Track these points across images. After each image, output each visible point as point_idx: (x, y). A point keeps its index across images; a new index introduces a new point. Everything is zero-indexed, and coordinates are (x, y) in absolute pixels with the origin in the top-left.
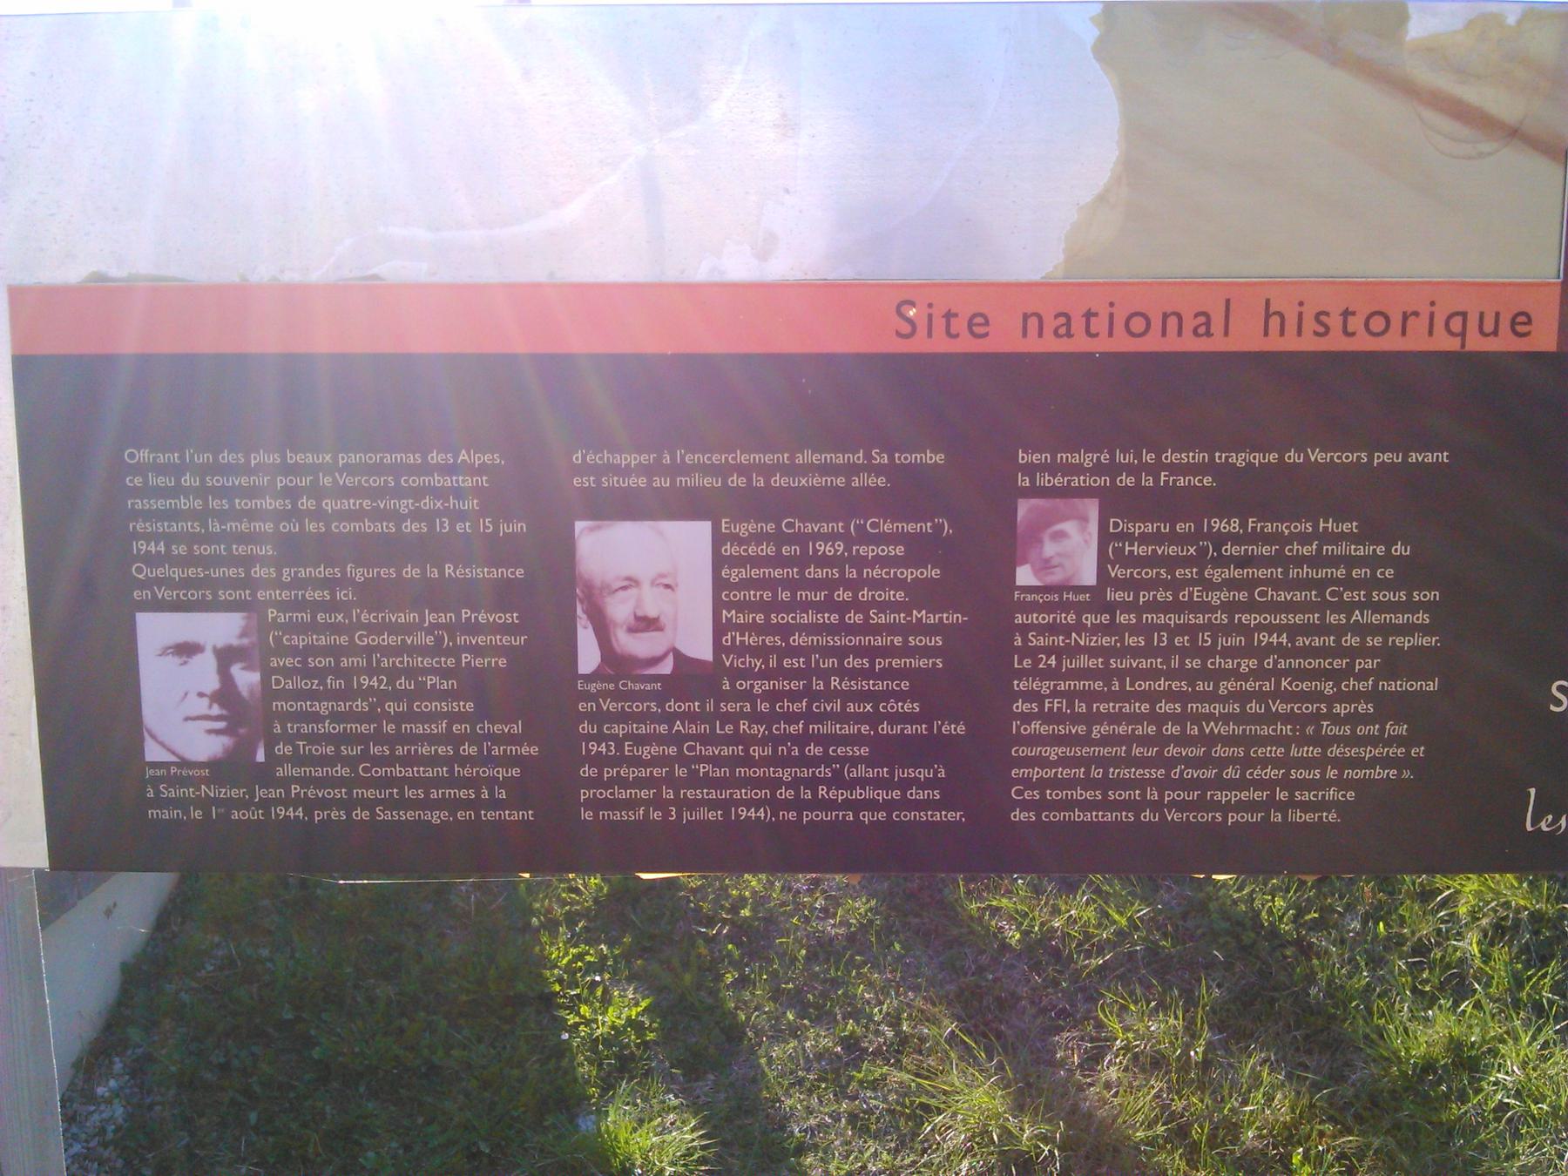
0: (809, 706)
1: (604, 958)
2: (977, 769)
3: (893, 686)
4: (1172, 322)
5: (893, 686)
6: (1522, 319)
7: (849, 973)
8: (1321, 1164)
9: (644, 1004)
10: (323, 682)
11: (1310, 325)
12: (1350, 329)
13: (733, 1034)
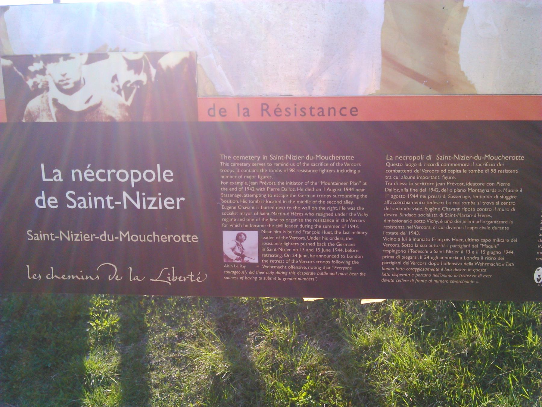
1: (111, 303)
2: (370, 245)
4: (332, 111)
6: (223, 110)
7: (188, 310)
8: (465, 380)
9: (117, 320)
10: (399, 214)
11: (299, 112)
12: (313, 114)
13: (144, 329)
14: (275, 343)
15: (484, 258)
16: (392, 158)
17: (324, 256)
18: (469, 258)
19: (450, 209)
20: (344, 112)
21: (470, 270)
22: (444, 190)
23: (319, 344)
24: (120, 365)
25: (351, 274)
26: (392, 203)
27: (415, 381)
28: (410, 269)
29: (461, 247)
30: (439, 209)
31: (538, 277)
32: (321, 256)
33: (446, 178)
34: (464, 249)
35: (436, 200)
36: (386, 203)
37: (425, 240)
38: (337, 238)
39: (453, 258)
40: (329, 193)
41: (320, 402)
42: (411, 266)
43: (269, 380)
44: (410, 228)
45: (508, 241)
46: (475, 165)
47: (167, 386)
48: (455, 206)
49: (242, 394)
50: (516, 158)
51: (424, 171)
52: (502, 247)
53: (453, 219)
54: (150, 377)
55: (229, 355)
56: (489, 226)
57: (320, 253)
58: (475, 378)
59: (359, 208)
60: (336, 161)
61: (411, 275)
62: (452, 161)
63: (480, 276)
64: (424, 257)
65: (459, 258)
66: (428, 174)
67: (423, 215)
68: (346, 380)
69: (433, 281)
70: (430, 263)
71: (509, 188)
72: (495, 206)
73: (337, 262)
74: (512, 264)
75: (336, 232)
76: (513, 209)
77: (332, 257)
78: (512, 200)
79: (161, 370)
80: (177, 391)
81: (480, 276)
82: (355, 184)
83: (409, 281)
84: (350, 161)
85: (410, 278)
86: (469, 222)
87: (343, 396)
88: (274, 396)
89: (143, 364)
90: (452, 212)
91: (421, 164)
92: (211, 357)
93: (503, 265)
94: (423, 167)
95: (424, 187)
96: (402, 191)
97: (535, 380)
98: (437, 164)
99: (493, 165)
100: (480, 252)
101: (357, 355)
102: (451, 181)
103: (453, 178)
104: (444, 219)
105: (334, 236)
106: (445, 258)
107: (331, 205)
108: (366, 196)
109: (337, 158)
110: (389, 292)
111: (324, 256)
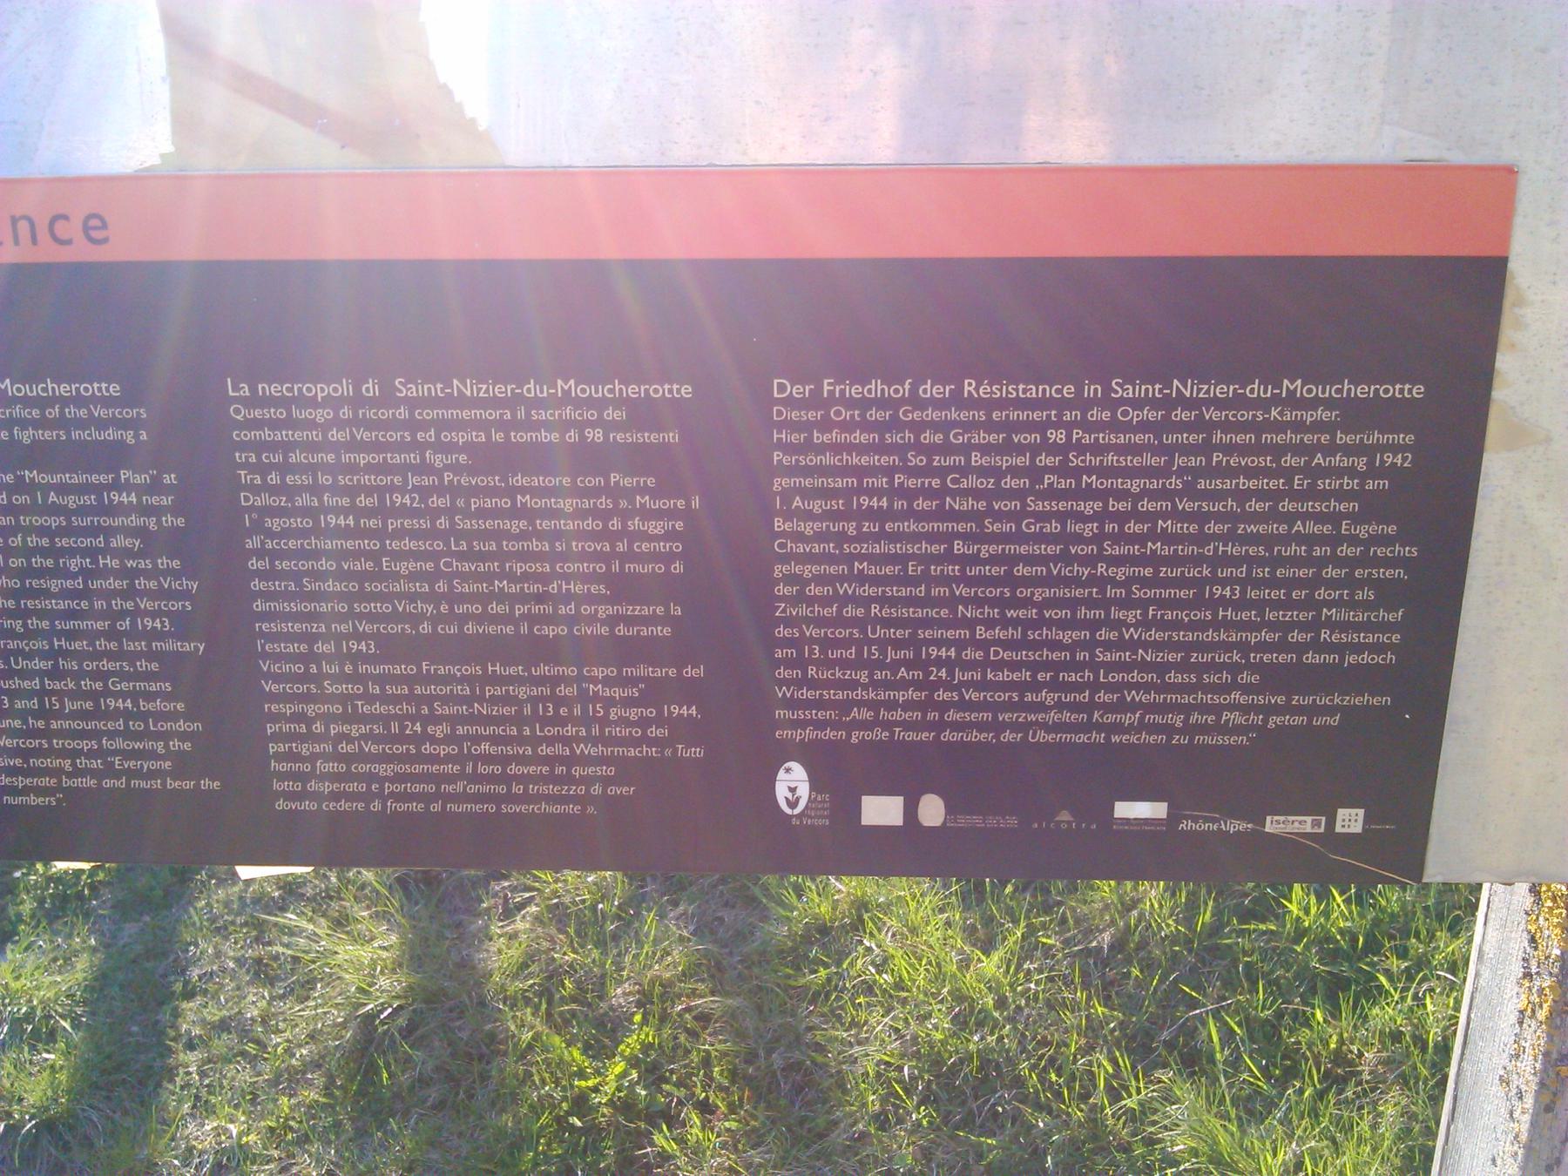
0: (840, 610)
3: (933, 613)
4: (23, 226)
5: (933, 613)
10: (299, 584)
14: (558, 915)
15: (602, 730)
16: (246, 391)
17: (74, 725)
18: (554, 731)
19: (467, 567)
20: (60, 227)
21: (560, 770)
22: (436, 502)
23: (693, 915)
24: (96, 979)
25: (172, 784)
26: (269, 545)
27: (939, 1025)
28: (364, 768)
29: (522, 692)
30: (429, 566)
31: (790, 795)
32: (66, 724)
33: (438, 460)
34: (534, 701)
35: (415, 534)
36: (249, 545)
37: (398, 670)
38: (106, 665)
39: (499, 731)
40: (56, 510)
41: (661, 1091)
42: (363, 757)
43: (524, 1026)
44: (343, 628)
45: (672, 672)
46: (528, 414)
47: (221, 1044)
48: (483, 557)
49: (437, 1069)
50: (1394, 390)
51: (363, 435)
52: (654, 693)
53: (484, 599)
54: (176, 1014)
55: (416, 956)
56: (603, 622)
57: (59, 715)
58: (1121, 1023)
59: (163, 562)
60: (64, 402)
61: (369, 787)
62: (448, 402)
63: (597, 789)
64: (403, 728)
65: (520, 731)
66: (377, 447)
67: (381, 587)
68: (750, 1023)
69: (444, 807)
70: (427, 748)
71: (655, 494)
72: (614, 554)
73: (119, 744)
74: (697, 752)
75: (101, 644)
76: (678, 567)
77: (101, 725)
78: (670, 536)
79: (215, 996)
80: (253, 1060)
81: (597, 789)
82: (140, 479)
83: (367, 807)
84: (107, 402)
85: (367, 797)
86: (535, 609)
87: (733, 1075)
88: (529, 1075)
89: (165, 976)
90: (478, 577)
91: (346, 413)
92: (361, 957)
93: (668, 752)
94: (355, 422)
95: (369, 491)
96: (299, 502)
97: (1292, 1032)
98: (402, 413)
99: (591, 415)
100: (585, 710)
101: (794, 949)
102: (456, 469)
103: (463, 458)
104: (453, 598)
105: (97, 656)
106: (472, 730)
107: (72, 552)
108: (180, 522)
109: (64, 390)
110: (335, 844)
111: (74, 725)
